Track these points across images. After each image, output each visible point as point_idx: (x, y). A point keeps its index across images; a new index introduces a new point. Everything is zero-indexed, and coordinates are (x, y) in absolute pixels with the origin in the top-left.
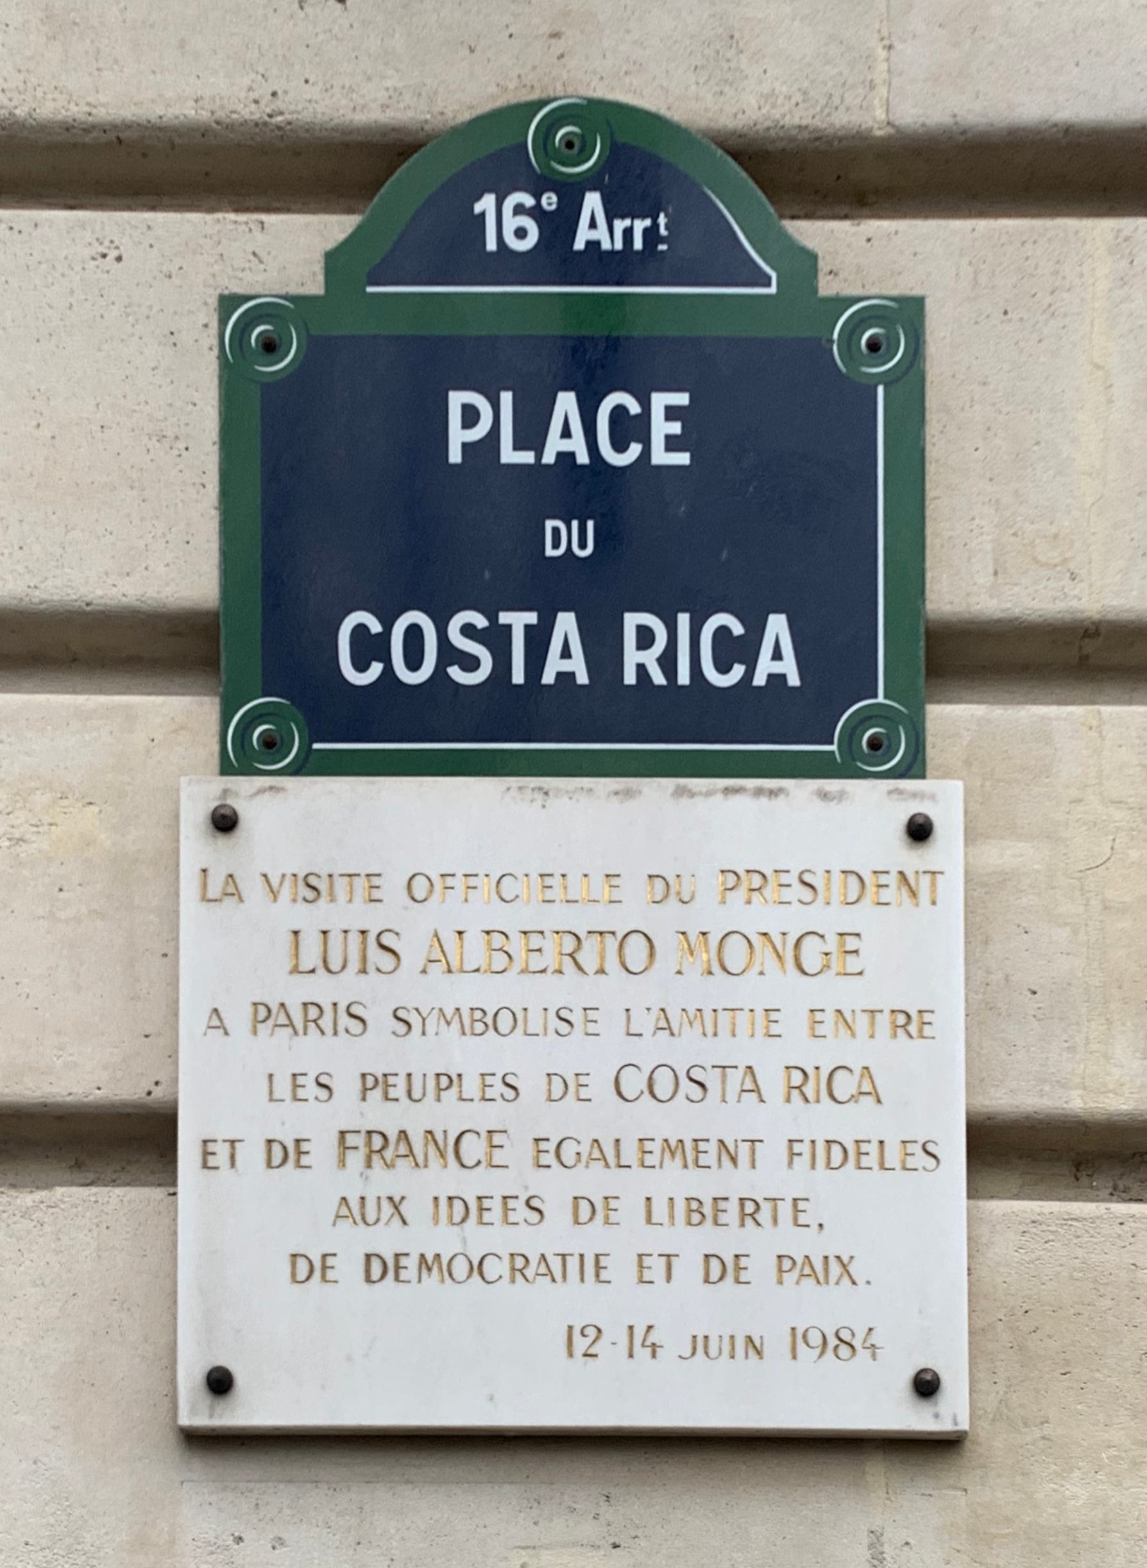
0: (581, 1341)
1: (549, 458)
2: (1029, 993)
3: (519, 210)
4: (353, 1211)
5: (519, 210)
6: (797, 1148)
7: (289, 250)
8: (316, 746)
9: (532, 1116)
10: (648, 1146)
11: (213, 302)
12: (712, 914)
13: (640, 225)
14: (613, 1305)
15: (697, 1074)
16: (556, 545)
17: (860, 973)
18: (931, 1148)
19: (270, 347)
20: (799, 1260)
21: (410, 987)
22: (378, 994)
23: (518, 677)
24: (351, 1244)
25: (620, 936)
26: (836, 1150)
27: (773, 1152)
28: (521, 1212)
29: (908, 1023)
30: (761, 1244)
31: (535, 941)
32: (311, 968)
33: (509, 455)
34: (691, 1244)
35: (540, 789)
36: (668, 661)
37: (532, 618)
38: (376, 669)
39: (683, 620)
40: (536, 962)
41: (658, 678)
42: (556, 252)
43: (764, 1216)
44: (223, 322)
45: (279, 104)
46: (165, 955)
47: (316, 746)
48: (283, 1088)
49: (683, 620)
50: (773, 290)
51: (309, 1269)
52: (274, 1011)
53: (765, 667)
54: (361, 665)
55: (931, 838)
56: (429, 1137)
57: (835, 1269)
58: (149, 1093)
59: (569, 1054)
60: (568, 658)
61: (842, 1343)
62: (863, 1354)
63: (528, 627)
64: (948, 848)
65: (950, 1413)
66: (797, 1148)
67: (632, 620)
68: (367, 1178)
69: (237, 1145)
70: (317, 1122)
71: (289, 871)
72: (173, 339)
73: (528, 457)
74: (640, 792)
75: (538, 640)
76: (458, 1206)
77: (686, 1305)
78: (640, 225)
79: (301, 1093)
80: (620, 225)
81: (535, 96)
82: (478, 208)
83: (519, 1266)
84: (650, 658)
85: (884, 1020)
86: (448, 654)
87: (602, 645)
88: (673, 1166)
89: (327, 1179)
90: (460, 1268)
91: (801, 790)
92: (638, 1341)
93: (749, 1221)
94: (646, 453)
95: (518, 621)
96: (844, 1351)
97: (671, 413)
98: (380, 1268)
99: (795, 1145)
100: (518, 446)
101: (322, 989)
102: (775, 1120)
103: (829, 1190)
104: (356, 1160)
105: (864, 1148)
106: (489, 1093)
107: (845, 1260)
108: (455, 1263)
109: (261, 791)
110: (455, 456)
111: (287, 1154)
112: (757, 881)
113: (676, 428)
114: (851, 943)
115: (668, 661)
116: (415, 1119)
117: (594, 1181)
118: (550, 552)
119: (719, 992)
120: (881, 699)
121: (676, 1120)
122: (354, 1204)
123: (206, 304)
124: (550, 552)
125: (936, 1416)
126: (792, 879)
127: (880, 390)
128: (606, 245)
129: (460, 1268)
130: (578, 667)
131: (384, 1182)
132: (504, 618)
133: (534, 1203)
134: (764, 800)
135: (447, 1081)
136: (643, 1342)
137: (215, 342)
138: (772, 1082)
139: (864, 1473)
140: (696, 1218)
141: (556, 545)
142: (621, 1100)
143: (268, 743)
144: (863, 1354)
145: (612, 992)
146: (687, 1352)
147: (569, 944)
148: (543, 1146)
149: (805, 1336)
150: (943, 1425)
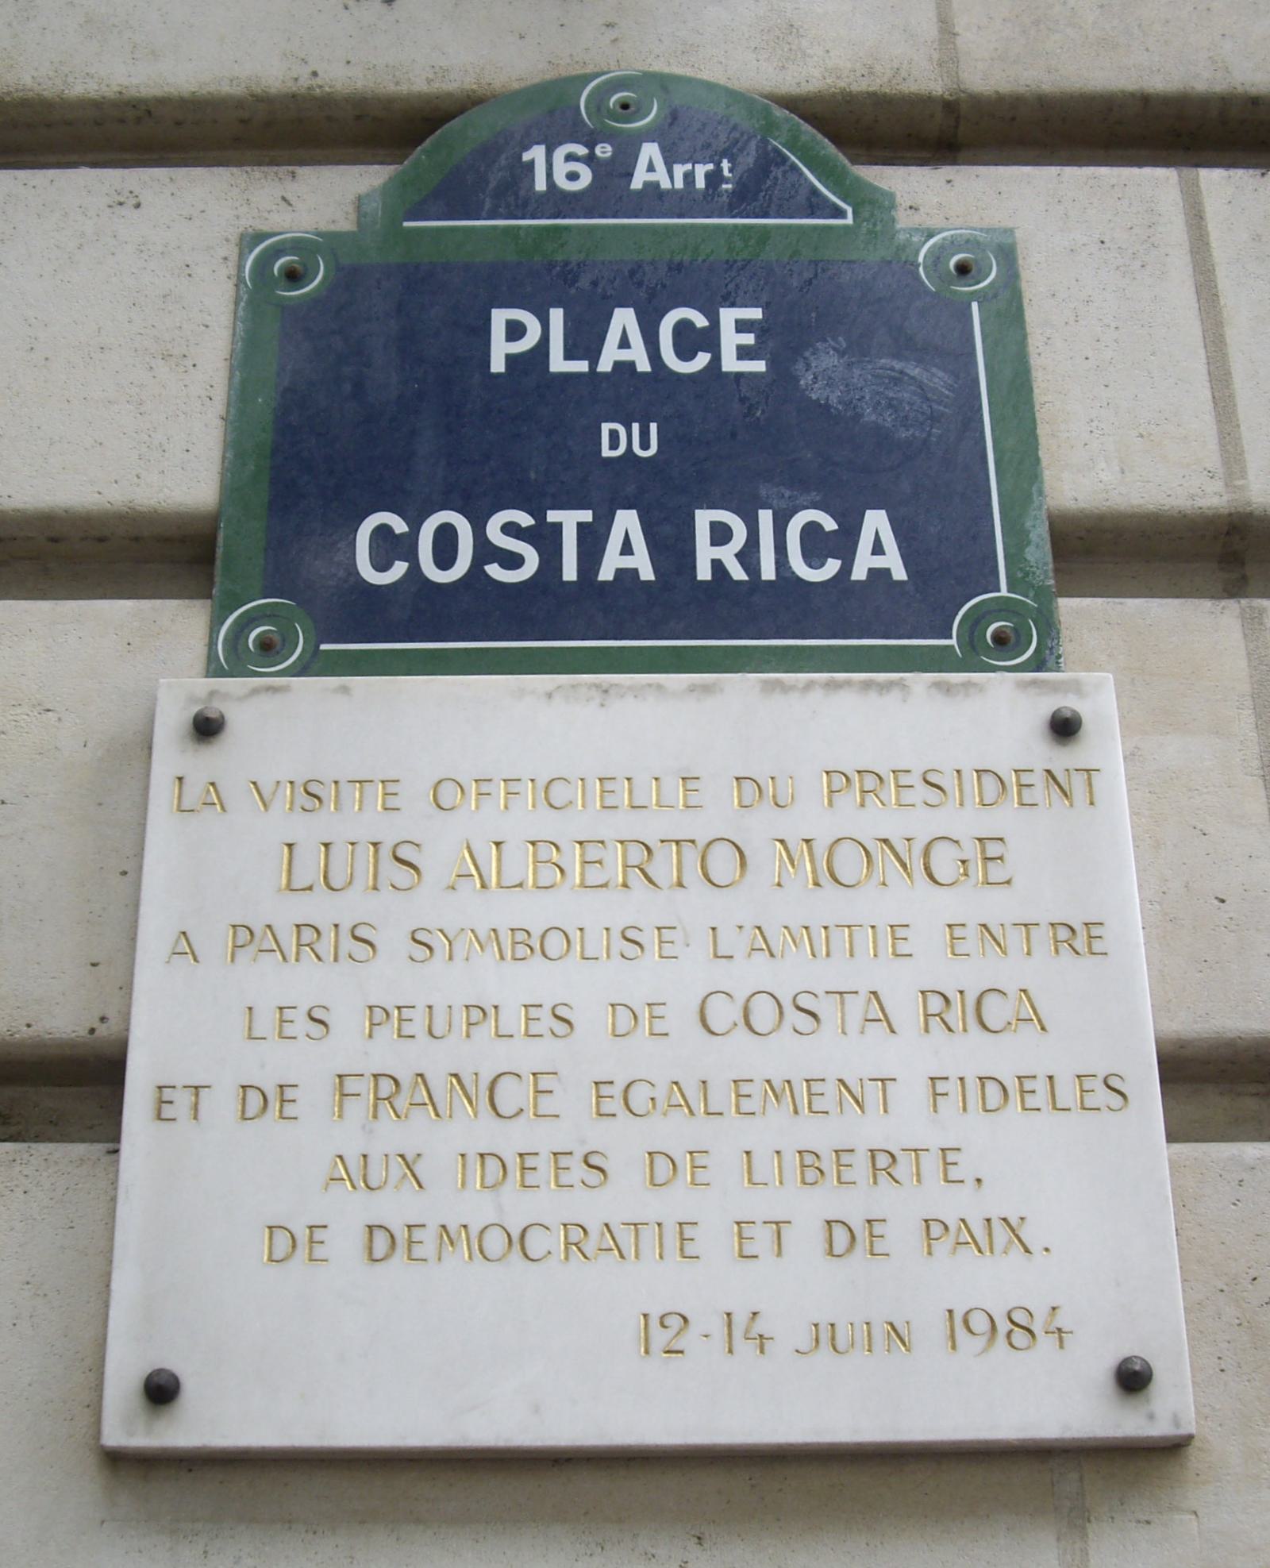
0: (665, 1332)
2: (1216, 902)
3: (570, 158)
4: (359, 1175)
6: (941, 1087)
7: (325, 200)
8: (323, 647)
9: (595, 1052)
10: (745, 1089)
11: (234, 239)
12: (814, 819)
13: (701, 171)
14: (711, 1286)
15: (805, 1001)
16: (614, 446)
17: (1008, 882)
18: (1115, 1082)
19: (293, 277)
20: (953, 1224)
21: (429, 906)
22: (392, 916)
23: (570, 573)
24: (347, 1215)
25: (701, 844)
26: (992, 1090)
27: (911, 1095)
28: (577, 1171)
29: (1078, 937)
30: (901, 1207)
31: (593, 853)
32: (306, 885)
33: (558, 363)
34: (809, 1209)
35: (597, 686)
36: (749, 556)
37: (587, 516)
38: (400, 569)
39: (765, 517)
40: (595, 876)
42: (611, 188)
43: (903, 1170)
44: (242, 257)
45: (319, 81)
46: (124, 873)
47: (323, 647)
48: (266, 1023)
49: (765, 517)
51: (293, 1243)
52: (258, 932)
53: (863, 564)
55: (1082, 732)
56: (454, 1081)
57: (1001, 1234)
58: (92, 1031)
59: (641, 980)
60: (627, 547)
61: (1017, 1329)
62: (1046, 1343)
63: (580, 525)
64: (1105, 745)
65: (1168, 1409)
66: (941, 1087)
67: (703, 519)
68: (371, 1132)
69: (203, 1092)
70: (307, 1064)
71: (284, 777)
72: (188, 271)
73: (582, 366)
74: (722, 690)
75: (592, 541)
76: (492, 1165)
77: (800, 1287)
79: (289, 1030)
80: (679, 170)
81: (588, 70)
83: (575, 1240)
84: (727, 554)
85: (1042, 935)
86: (485, 552)
87: (671, 544)
88: (778, 1116)
89: (321, 1133)
90: (495, 1242)
91: (920, 681)
92: (738, 1333)
93: (883, 1177)
94: (716, 359)
95: (569, 520)
96: (1019, 1337)
97: (742, 326)
98: (382, 1243)
99: (939, 1083)
100: (569, 356)
101: (320, 909)
102: (911, 1055)
103: (979, 1136)
104: (357, 1110)
105: (1028, 1085)
106: (535, 1028)
107: (1014, 1222)
108: (487, 1236)
109: (255, 691)
110: (498, 365)
111: (266, 1101)
112: (870, 782)
113: (749, 339)
114: (993, 850)
115: (749, 556)
116: (437, 1061)
117: (673, 1133)
118: (606, 452)
119: (831, 905)
120: (1004, 592)
121: (782, 1055)
122: (355, 1164)
123: (227, 240)
124: (606, 452)
125: (1151, 1417)
126: (915, 779)
127: (975, 306)
128: (665, 184)
129: (495, 1242)
130: (642, 564)
131: (393, 1135)
132: (553, 516)
133: (594, 1160)
134: (873, 694)
135: (479, 1013)
136: (745, 1332)
137: (234, 272)
138: (906, 1010)
139: (1084, 1536)
140: (811, 1174)
141: (614, 446)
142: (704, 1031)
143: (266, 646)
144: (1046, 1343)
145: (697, 906)
146: (805, 1343)
147: (637, 855)
148: (605, 1090)
149: (966, 1322)
150: (1161, 1428)
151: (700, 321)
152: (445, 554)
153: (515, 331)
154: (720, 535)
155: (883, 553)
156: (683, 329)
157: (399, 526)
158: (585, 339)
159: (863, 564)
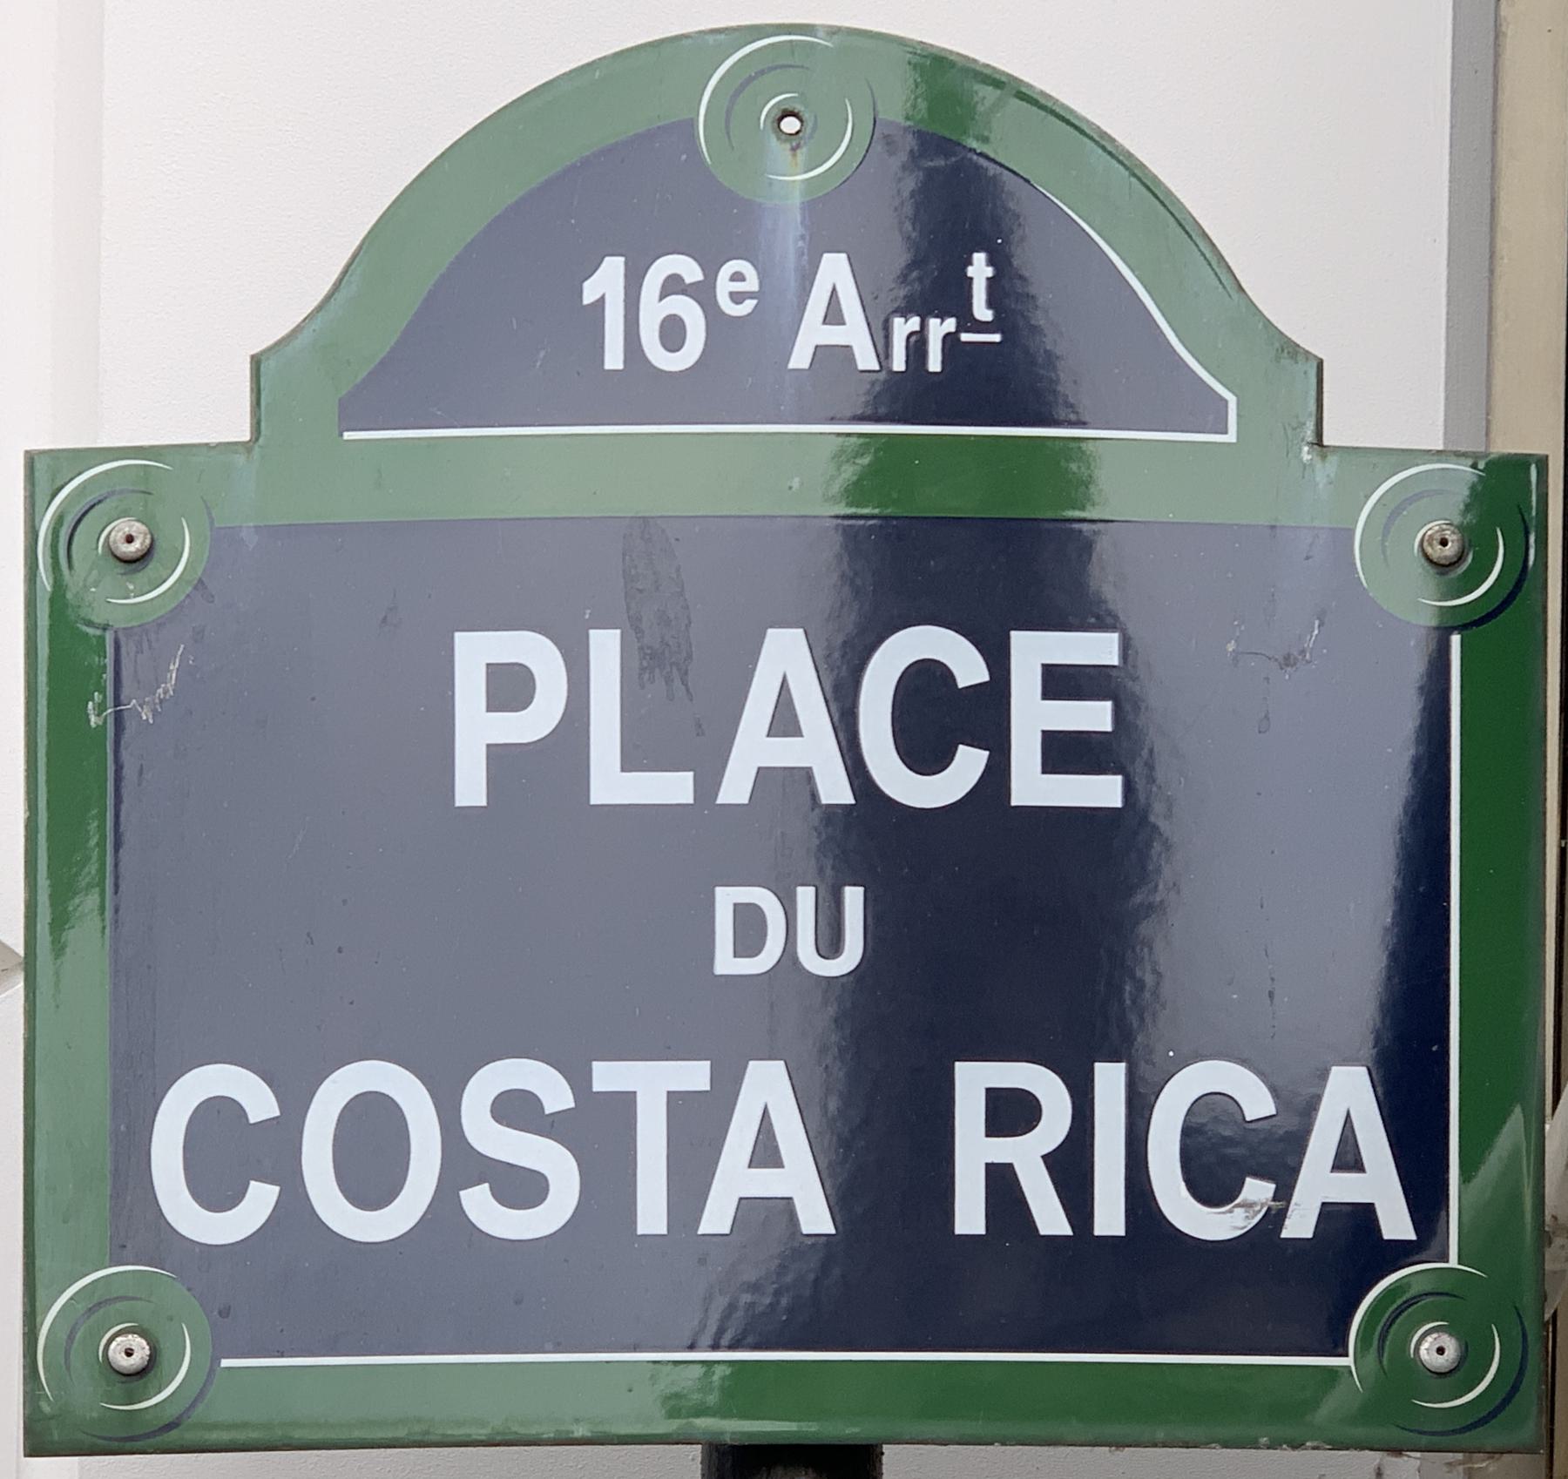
1: (735, 788)
13: (939, 329)
23: (652, 1216)
33: (612, 783)
36: (1071, 1168)
37: (695, 1076)
38: (261, 1199)
41: (1051, 1218)
49: (1110, 1079)
50: (1231, 437)
63: (677, 1102)
67: (973, 1082)
73: (675, 788)
84: (1027, 1155)
86: (462, 1164)
94: (997, 774)
95: (653, 1084)
100: (632, 760)
115: (1071, 1168)
118: (726, 962)
124: (726, 962)
132: (607, 1076)
152: (371, 1179)
153: (510, 687)
154: (1011, 1112)
156: (923, 686)
158: (682, 708)
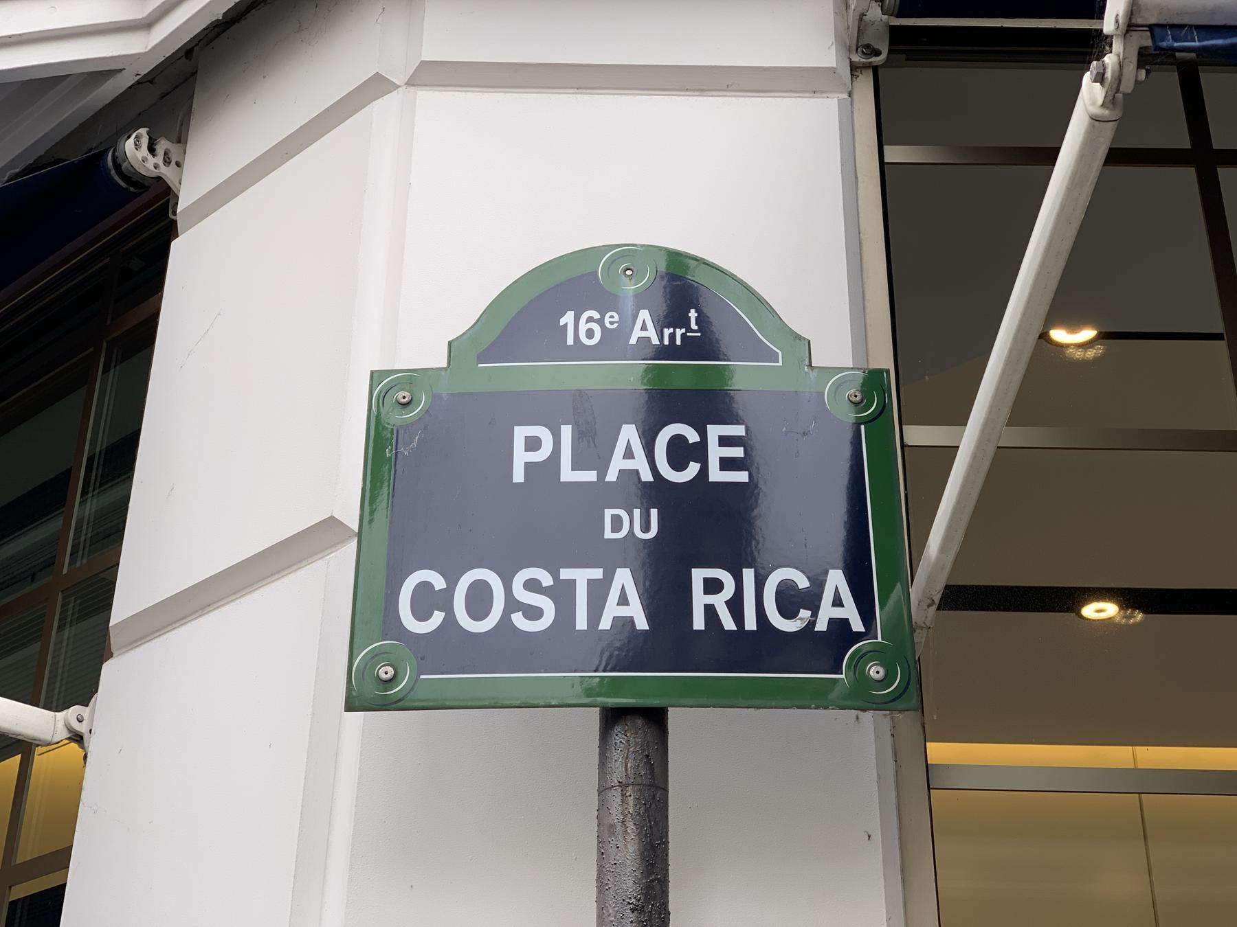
1: (611, 476)
3: (590, 319)
5: (590, 319)
13: (679, 332)
23: (581, 623)
36: (736, 605)
37: (597, 573)
38: (438, 617)
39: (748, 575)
41: (729, 624)
49: (748, 575)
50: (780, 364)
53: (827, 613)
54: (421, 613)
73: (590, 476)
75: (598, 592)
78: (679, 332)
82: (562, 322)
84: (719, 601)
86: (512, 604)
94: (704, 471)
95: (581, 577)
110: (519, 476)
115: (736, 605)
118: (608, 534)
124: (608, 534)
151: (693, 437)
154: (713, 586)
155: (841, 605)
156: (677, 443)
157: (439, 583)
159: (827, 613)
